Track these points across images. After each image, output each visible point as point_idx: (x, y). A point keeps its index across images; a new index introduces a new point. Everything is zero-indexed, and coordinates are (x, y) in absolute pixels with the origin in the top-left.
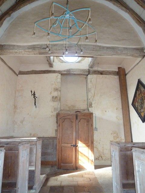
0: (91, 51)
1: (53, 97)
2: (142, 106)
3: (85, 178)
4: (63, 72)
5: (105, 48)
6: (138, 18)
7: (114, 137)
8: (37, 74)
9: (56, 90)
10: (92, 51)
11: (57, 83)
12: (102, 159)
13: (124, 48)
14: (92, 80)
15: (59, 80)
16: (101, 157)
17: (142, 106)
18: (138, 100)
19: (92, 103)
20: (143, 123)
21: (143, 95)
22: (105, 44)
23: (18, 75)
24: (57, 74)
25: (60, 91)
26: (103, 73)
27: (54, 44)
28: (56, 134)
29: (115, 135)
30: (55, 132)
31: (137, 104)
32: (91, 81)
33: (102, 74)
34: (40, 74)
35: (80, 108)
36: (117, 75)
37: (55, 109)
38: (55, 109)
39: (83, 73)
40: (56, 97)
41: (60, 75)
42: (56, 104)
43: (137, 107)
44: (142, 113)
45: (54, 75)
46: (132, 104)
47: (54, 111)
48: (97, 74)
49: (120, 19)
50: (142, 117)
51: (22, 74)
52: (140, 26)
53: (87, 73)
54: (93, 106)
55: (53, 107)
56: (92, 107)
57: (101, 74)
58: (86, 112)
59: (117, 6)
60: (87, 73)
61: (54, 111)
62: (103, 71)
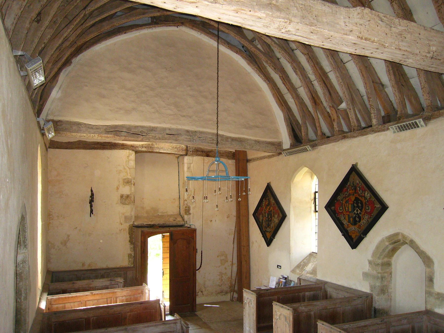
0: (209, 143)
1: (122, 196)
2: (268, 223)
3: (405, 321)
4: (140, 149)
5: (229, 140)
6: (279, 98)
7: (221, 260)
8: (88, 149)
9: (127, 182)
10: (210, 144)
11: (129, 168)
12: (203, 294)
13: (256, 141)
14: (192, 165)
15: (132, 164)
16: (202, 292)
17: (268, 223)
18: (263, 212)
19: (189, 207)
20: (268, 246)
21: (272, 208)
22: (229, 132)
23: (49, 149)
24: (128, 151)
25: (134, 185)
26: (210, 154)
27: (150, 127)
28: (129, 261)
29: (223, 258)
30: (128, 258)
31: (261, 218)
32: (189, 168)
33: (208, 156)
34: (95, 151)
35: (167, 212)
36: (233, 158)
37: (126, 219)
38: (126, 218)
39: (176, 151)
40: (128, 196)
41: (134, 153)
42: (127, 210)
43: (261, 221)
44: (268, 233)
45: (126, 152)
46: (254, 215)
47: (126, 222)
48: (200, 155)
49: (252, 89)
50: (267, 238)
51: (57, 148)
52: (280, 109)
53: (184, 153)
54: (191, 212)
55: (123, 214)
56: (190, 214)
57: (207, 156)
58: (179, 221)
59: (253, 69)
60: (184, 153)
61: (126, 222)
62: (211, 151)
